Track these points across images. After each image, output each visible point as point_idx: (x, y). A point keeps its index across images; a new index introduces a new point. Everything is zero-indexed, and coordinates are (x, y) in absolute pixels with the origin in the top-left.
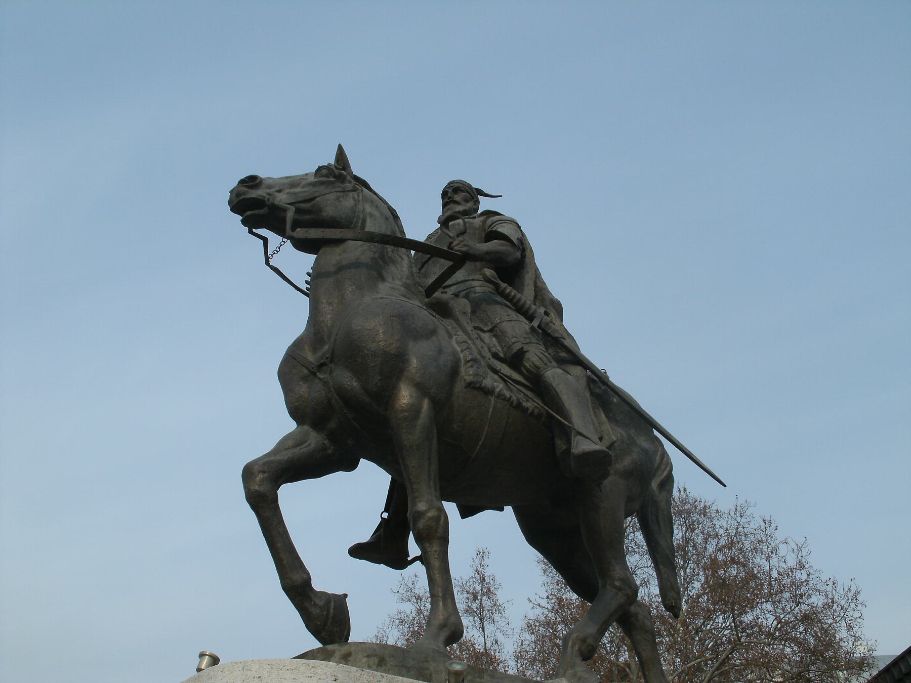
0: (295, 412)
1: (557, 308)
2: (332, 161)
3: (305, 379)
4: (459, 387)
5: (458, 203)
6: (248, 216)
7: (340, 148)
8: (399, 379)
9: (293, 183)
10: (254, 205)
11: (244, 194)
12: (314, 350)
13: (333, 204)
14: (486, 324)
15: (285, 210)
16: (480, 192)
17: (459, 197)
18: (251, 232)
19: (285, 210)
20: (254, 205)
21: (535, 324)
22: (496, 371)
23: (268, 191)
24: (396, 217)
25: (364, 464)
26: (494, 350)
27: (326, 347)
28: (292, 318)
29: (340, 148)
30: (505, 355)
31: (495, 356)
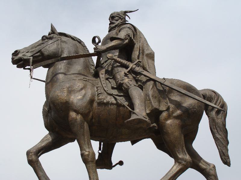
0: (47, 127)
2: (49, 30)
4: (95, 104)
7: (51, 23)
13: (51, 47)
18: (24, 69)
20: (20, 61)
28: (38, 97)
29: (51, 23)
31: (113, 88)
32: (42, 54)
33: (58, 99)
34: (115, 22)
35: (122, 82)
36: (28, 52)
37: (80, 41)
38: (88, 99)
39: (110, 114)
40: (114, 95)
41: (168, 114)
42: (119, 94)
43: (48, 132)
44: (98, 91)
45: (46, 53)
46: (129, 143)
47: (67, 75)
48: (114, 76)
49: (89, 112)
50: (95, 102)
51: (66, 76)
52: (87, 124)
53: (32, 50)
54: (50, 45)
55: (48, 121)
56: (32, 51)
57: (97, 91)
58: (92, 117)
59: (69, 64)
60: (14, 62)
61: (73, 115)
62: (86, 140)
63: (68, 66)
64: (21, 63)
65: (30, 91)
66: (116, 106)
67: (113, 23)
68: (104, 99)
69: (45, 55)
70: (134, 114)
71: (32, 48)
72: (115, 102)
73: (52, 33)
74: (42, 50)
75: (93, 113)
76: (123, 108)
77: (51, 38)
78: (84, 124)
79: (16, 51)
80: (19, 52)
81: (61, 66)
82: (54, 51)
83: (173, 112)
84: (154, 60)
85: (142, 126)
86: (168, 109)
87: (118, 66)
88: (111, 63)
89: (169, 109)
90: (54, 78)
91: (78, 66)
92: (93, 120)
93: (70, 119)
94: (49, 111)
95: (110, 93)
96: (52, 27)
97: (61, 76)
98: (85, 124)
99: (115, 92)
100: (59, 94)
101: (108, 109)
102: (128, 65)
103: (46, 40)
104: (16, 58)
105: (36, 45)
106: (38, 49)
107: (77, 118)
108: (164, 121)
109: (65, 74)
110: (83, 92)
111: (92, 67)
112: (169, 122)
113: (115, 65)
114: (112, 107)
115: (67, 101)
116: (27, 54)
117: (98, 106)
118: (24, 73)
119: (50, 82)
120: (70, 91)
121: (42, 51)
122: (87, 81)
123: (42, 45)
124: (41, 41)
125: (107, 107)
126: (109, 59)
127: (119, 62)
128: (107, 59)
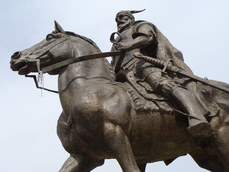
0: (67, 149)
1: (180, 55)
2: (54, 29)
4: (133, 113)
6: (21, 70)
7: (55, 22)
9: (38, 47)
11: (15, 62)
12: (66, 120)
13: (59, 48)
14: (143, 78)
15: (35, 62)
16: (133, 12)
17: (124, 19)
18: (26, 76)
19: (35, 62)
20: (22, 66)
21: (164, 70)
22: (150, 100)
23: (26, 56)
24: (91, 42)
25: (106, 161)
26: (148, 89)
28: (54, 108)
29: (55, 22)
30: (153, 90)
31: (149, 92)
32: (51, 56)
33: (88, 107)
34: (123, 21)
35: (161, 84)
36: (31, 54)
37: (91, 41)
38: (125, 105)
39: (154, 124)
40: (153, 99)
41: (219, 120)
42: (160, 99)
43: (69, 154)
44: (134, 96)
45: (56, 54)
46: (162, 163)
47: (88, 79)
48: (147, 77)
49: (128, 122)
50: (132, 110)
51: (88, 80)
52: (127, 137)
53: (38, 51)
54: (60, 45)
55: (71, 139)
56: (37, 53)
57: (131, 96)
58: (132, 128)
59: (86, 66)
60: (15, 67)
61: (109, 126)
62: (130, 158)
63: (86, 68)
64: (23, 68)
65: (42, 103)
66: (159, 113)
67: (123, 23)
68: (144, 105)
69: (54, 57)
70: (192, 119)
71: (36, 49)
72: (157, 108)
73: (57, 32)
74: (50, 51)
75: (132, 123)
76: (168, 115)
77: (58, 37)
78: (125, 138)
79: (17, 53)
80: (21, 54)
81: (77, 69)
82: (66, 51)
83: (224, 118)
84: (183, 60)
85: (204, 134)
86: (218, 115)
87: (147, 67)
88: (134, 65)
89: (219, 114)
90: (72, 83)
91: (97, 68)
92: (133, 132)
93: (106, 132)
94: (70, 126)
95: (148, 98)
96: (56, 25)
97: (80, 81)
98: (126, 138)
99: (153, 97)
100: (87, 101)
101: (150, 117)
102: (163, 64)
103: (53, 39)
104: (18, 61)
105: (41, 45)
106: (45, 49)
107: (116, 131)
108: (216, 129)
109: (85, 78)
110: (116, 97)
111: (112, 71)
112: (221, 130)
113: (144, 66)
114: (155, 114)
115: (100, 110)
116: (31, 56)
117: (138, 115)
118: (25, 82)
119: (65, 91)
120: (101, 97)
121: (50, 52)
122: (115, 85)
123: (49, 45)
124: (46, 41)
125: (148, 115)
126: (135, 57)
127: (148, 61)
128: (133, 57)
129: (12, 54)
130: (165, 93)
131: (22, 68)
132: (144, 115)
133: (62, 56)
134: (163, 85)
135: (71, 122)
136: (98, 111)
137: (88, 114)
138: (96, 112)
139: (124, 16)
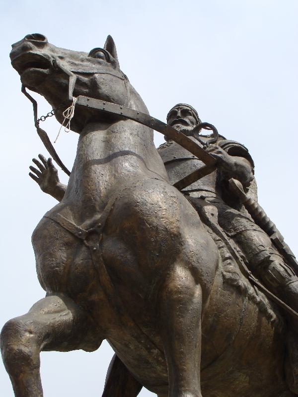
0: (52, 279)
3: (67, 245)
5: (186, 124)
8: (174, 260)
10: (35, 66)
11: (31, 49)
12: (81, 219)
18: (23, 91)
20: (35, 66)
23: (53, 54)
27: (98, 216)
35: (271, 259)
61: (181, 275)
96: (110, 43)
103: (105, 61)
125: (241, 299)
129: (31, 33)
130: (273, 279)
131: (38, 69)
132: (234, 296)
133: (113, 99)
134: (272, 261)
135: (99, 227)
136: (175, 235)
137: (157, 228)
138: (173, 233)
139: (191, 115)
